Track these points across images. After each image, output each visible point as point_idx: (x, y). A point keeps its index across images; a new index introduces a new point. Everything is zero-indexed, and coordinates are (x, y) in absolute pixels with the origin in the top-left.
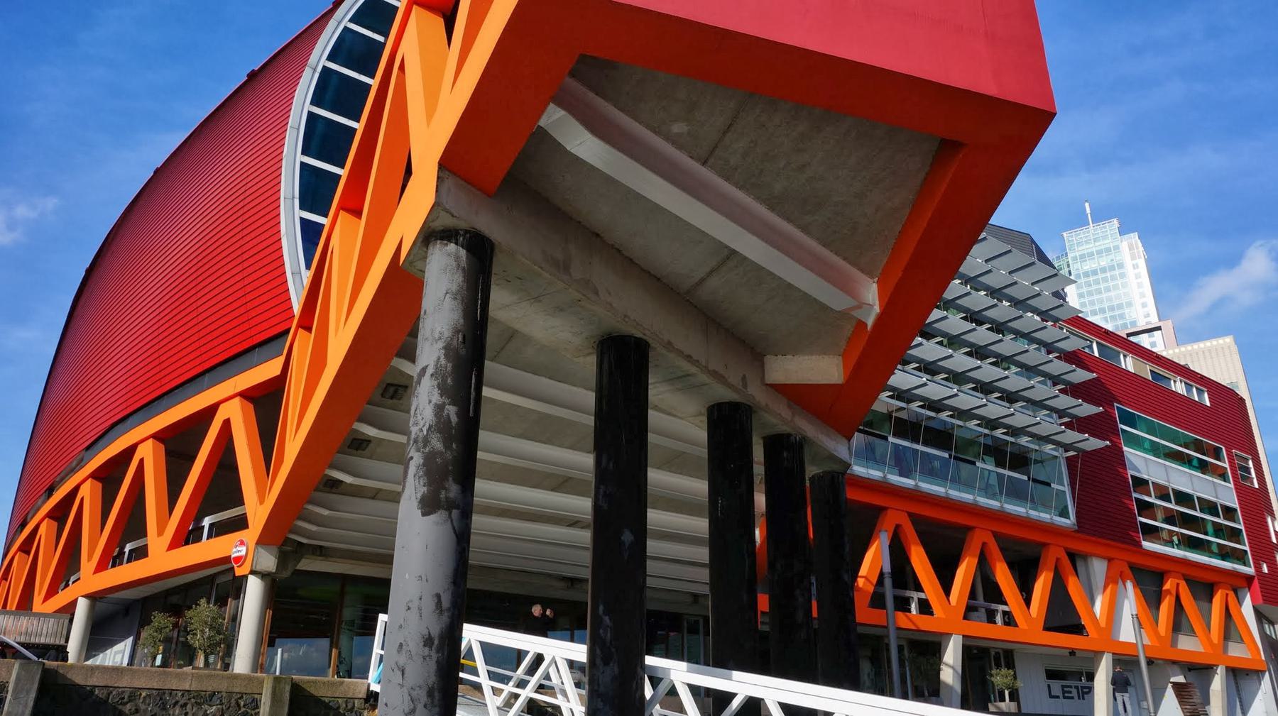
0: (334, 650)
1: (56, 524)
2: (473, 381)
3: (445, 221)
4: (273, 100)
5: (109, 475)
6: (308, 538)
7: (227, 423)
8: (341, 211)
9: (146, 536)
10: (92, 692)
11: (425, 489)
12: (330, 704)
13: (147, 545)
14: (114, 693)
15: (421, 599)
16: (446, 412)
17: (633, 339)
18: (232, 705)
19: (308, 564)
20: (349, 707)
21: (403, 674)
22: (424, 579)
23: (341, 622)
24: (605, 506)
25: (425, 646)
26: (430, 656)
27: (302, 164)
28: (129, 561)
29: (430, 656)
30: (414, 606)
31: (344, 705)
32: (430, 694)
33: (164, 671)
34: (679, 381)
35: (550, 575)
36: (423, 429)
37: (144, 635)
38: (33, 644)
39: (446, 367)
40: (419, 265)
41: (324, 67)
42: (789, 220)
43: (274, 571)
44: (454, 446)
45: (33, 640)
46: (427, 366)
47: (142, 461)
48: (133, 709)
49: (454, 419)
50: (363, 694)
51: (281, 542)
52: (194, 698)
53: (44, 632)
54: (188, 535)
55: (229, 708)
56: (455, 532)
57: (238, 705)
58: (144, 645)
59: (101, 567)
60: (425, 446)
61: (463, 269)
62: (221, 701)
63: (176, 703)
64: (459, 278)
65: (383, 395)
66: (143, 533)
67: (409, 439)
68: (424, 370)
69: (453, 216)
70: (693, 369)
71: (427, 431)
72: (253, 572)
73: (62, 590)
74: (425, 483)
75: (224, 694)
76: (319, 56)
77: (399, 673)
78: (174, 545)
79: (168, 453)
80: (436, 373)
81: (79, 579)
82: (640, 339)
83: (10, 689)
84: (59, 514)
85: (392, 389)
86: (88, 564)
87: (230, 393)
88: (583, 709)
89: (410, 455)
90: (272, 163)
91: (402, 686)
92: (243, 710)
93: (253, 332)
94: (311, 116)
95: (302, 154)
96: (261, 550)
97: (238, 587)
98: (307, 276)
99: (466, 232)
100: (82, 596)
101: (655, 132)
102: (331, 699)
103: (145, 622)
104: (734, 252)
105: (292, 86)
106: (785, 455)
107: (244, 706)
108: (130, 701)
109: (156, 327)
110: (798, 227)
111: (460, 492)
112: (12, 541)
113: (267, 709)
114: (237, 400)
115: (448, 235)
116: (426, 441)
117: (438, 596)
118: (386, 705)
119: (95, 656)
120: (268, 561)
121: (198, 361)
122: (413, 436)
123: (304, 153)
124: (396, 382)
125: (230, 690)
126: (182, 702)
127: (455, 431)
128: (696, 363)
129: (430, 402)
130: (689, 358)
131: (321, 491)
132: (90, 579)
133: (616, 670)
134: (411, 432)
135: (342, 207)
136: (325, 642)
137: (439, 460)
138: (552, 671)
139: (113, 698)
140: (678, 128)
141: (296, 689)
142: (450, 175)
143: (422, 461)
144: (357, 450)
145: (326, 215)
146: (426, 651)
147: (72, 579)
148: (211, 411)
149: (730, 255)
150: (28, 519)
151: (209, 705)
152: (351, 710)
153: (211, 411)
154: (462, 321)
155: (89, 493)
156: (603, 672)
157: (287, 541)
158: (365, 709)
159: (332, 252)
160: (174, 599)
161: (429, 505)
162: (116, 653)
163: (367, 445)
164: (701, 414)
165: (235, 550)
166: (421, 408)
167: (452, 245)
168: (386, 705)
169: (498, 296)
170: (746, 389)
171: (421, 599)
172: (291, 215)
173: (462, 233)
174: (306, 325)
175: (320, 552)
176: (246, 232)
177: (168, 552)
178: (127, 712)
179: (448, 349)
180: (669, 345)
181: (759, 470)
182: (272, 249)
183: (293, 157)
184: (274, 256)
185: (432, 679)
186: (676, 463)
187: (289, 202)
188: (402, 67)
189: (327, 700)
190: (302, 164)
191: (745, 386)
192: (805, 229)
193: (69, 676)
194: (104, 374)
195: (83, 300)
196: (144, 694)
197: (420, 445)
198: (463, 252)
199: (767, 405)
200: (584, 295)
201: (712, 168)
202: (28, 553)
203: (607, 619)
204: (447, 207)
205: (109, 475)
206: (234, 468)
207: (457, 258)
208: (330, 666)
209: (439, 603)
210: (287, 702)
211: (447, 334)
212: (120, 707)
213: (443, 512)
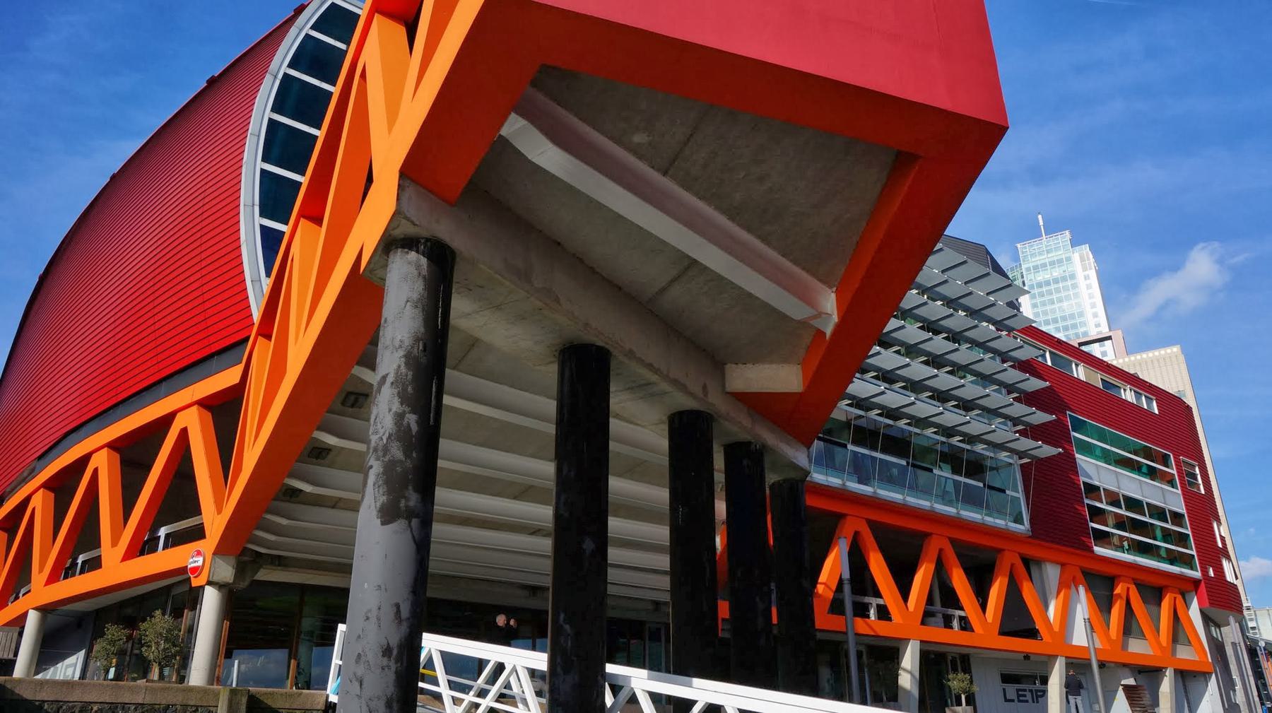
0: (292, 661)
2: (434, 389)
3: (405, 229)
4: (179, 196)
5: (62, 485)
7: (184, 432)
10: (41, 707)
11: (385, 498)
13: (100, 556)
14: (64, 707)
16: (406, 420)
19: (266, 574)
21: (361, 685)
25: (383, 656)
26: (389, 667)
28: (82, 572)
29: (389, 667)
34: (640, 389)
37: (96, 648)
39: (407, 376)
41: (285, 75)
44: (414, 455)
47: (96, 470)
49: (414, 428)
54: (143, 546)
59: (52, 579)
60: (384, 456)
61: (424, 277)
65: (343, 403)
66: (97, 545)
68: (384, 378)
69: (415, 225)
70: (654, 378)
72: (210, 583)
73: (12, 602)
75: (179, 707)
76: (281, 63)
77: (357, 684)
78: (128, 556)
79: (124, 462)
81: (29, 591)
85: (352, 398)
86: (38, 577)
87: (189, 402)
89: (370, 464)
91: (359, 697)
96: (219, 561)
97: (194, 598)
98: (267, 284)
99: (427, 240)
100: (33, 609)
103: (99, 633)
104: (694, 262)
114: (195, 408)
115: (409, 243)
116: (386, 450)
117: (398, 606)
120: (226, 572)
123: (265, 159)
124: (357, 391)
125: (185, 702)
128: (657, 371)
130: (650, 366)
134: (370, 441)
140: (639, 138)
143: (382, 470)
146: (385, 661)
147: (23, 591)
149: (691, 265)
153: (167, 420)
154: (422, 330)
155: (40, 504)
159: (292, 260)
160: (129, 611)
161: (388, 514)
162: (68, 666)
164: (663, 422)
165: (191, 560)
169: (459, 304)
171: (379, 609)
173: (423, 241)
175: (279, 562)
179: (408, 356)
180: (630, 354)
181: (719, 477)
184: (236, 272)
185: (391, 690)
186: (635, 470)
187: (249, 209)
192: (765, 239)
195: (35, 307)
197: (380, 453)
198: (424, 261)
203: (567, 627)
205: (62, 485)
207: (418, 267)
208: (288, 678)
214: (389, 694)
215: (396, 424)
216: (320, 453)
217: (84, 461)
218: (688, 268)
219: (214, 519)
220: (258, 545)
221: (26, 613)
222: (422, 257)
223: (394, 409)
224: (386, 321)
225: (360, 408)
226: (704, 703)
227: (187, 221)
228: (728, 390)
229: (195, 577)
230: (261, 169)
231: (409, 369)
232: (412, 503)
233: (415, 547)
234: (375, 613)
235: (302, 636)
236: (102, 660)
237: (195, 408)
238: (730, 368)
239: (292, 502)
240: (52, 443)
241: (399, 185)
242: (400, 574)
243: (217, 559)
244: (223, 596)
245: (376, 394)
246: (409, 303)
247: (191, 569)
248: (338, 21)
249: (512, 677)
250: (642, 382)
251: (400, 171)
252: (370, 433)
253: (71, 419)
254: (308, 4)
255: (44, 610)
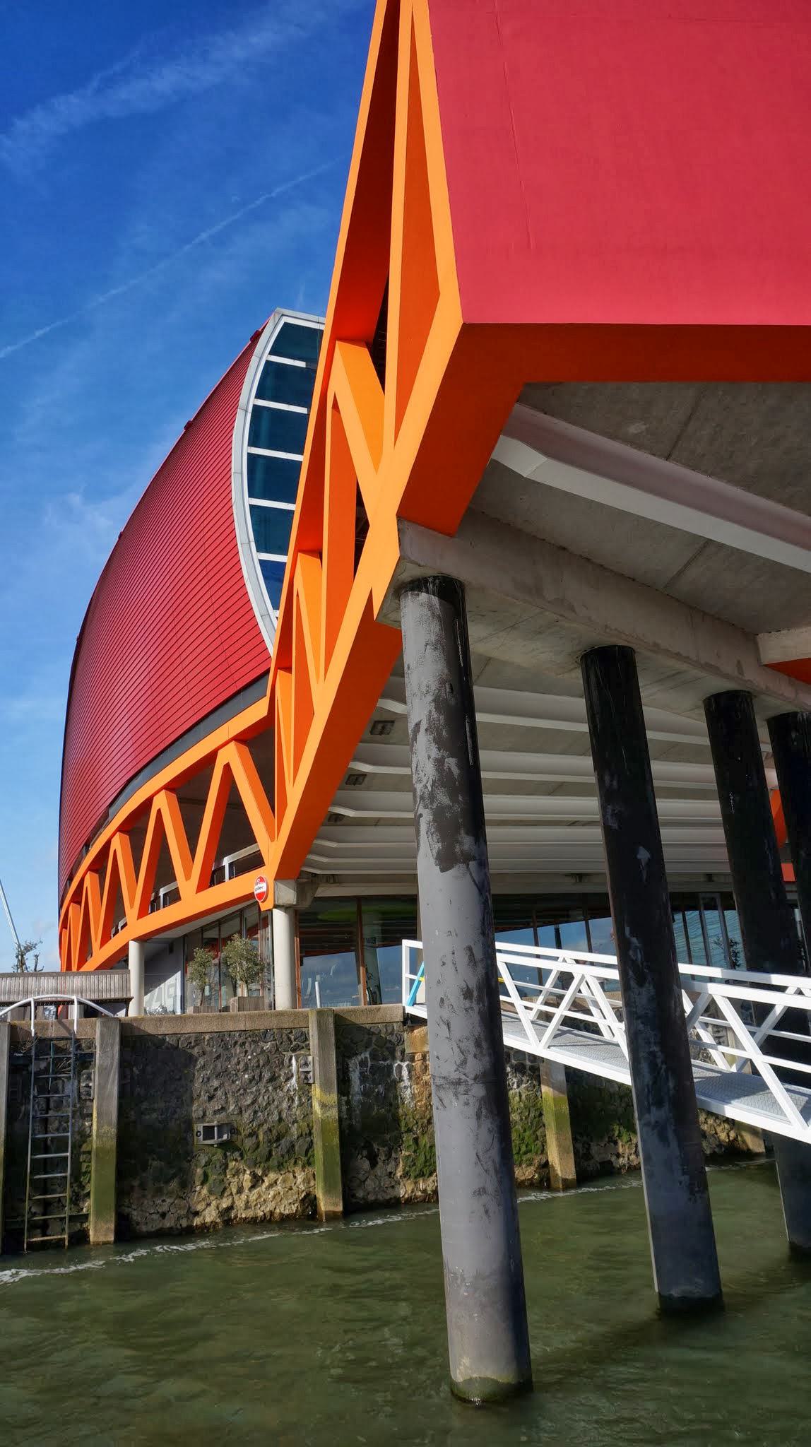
0: (361, 968)
1: (97, 876)
2: (468, 729)
3: (412, 572)
5: (134, 826)
6: (321, 869)
7: (227, 768)
8: (299, 554)
9: (176, 880)
10: (164, 1040)
11: (440, 845)
12: (372, 1030)
14: (182, 1039)
15: (453, 953)
16: (446, 765)
17: (617, 648)
18: (284, 1040)
19: (324, 891)
20: (389, 1031)
21: (449, 1028)
22: (453, 934)
23: (362, 942)
24: (615, 826)
25: (465, 998)
26: (472, 1008)
27: (252, 507)
29: (472, 1008)
30: (448, 961)
31: (385, 1030)
32: (478, 1044)
33: (221, 1015)
34: (671, 679)
35: (556, 874)
36: (427, 785)
37: (190, 970)
38: (106, 1000)
39: (439, 720)
40: (393, 616)
41: (255, 406)
42: (768, 496)
43: (295, 903)
44: (460, 798)
45: (104, 997)
46: (420, 721)
47: (159, 811)
48: (201, 1051)
49: (456, 771)
50: (400, 1018)
51: (296, 877)
52: (250, 1036)
53: (113, 988)
54: (212, 877)
55: (282, 1043)
56: (475, 884)
57: (289, 1039)
58: (192, 979)
59: (142, 914)
60: (432, 803)
61: (439, 617)
62: (274, 1037)
63: (236, 1043)
64: (435, 627)
65: (372, 732)
66: (173, 878)
67: (415, 796)
68: (418, 725)
69: (419, 566)
70: (684, 667)
71: (432, 787)
72: (276, 906)
73: (114, 935)
74: (438, 839)
75: (275, 1031)
76: (248, 396)
77: (445, 1027)
78: (201, 887)
79: (181, 801)
80: (430, 727)
82: (623, 647)
83: (98, 1044)
84: (98, 866)
85: (379, 727)
86: (131, 911)
87: (226, 739)
88: (623, 1026)
89: (419, 813)
90: (223, 511)
91: (449, 1039)
92: (294, 1043)
93: (236, 677)
94: (252, 458)
95: (249, 497)
96: (281, 886)
97: (266, 920)
98: (277, 615)
99: (435, 578)
100: (132, 940)
101: (610, 438)
102: (371, 1025)
103: (189, 958)
104: (709, 542)
105: (228, 432)
106: (793, 736)
107: (295, 1040)
108: (197, 1045)
109: (149, 685)
110: (780, 501)
111: (473, 843)
112: (63, 896)
113: (316, 1041)
114: (233, 743)
115: (417, 585)
116: (432, 797)
117: (470, 949)
118: (438, 1057)
119: (152, 991)
120: (288, 895)
121: (191, 712)
122: (419, 793)
123: (251, 495)
124: (383, 719)
125: (280, 1026)
126: (240, 1041)
127: (459, 783)
128: (686, 659)
129: (429, 757)
130: (678, 656)
131: (326, 825)
132: (136, 925)
133: (652, 991)
134: (415, 789)
135: (299, 550)
136: (351, 956)
137: (448, 815)
138: (583, 988)
139: (182, 1044)
140: (634, 429)
141: (339, 1020)
142: (409, 524)
143: (432, 817)
144: (354, 785)
145: (286, 553)
146: (467, 1003)
147: (121, 924)
148: (211, 758)
149: (706, 545)
150: (74, 873)
151: (264, 1042)
152: (392, 1033)
153: (211, 758)
154: (446, 671)
155: (119, 845)
156: (639, 994)
157: (301, 874)
158: (404, 1031)
159: (298, 595)
160: (212, 934)
161: (446, 861)
162: (169, 987)
163: (363, 780)
164: (697, 707)
165: (256, 887)
166: (421, 764)
167: (424, 594)
168: (438, 1057)
169: (475, 631)
170: (743, 675)
171: (453, 953)
172: (250, 559)
173: (430, 580)
174: (284, 663)
175: (333, 879)
176: (209, 567)
177: (140, 920)
178: (196, 1054)
179: (437, 701)
180: (656, 648)
181: (766, 748)
182: (240, 603)
183: (242, 502)
184: (247, 617)
185: (478, 1030)
186: (676, 752)
187: (246, 547)
188: (335, 406)
189: (367, 1026)
190: (252, 507)
191: (741, 673)
192: (788, 503)
193: (142, 1027)
194: (111, 736)
195: (80, 666)
196: (207, 1037)
197: (428, 801)
198: (435, 600)
199: (767, 687)
200: (561, 616)
201: (677, 461)
202: (79, 903)
203: (634, 940)
204: (413, 559)
205: (134, 826)
206: (240, 806)
207: (431, 607)
208: (359, 983)
209: (472, 956)
210: (333, 1033)
211: (434, 686)
212: (189, 1051)
213: (461, 865)
214: (476, 1034)
215: (437, 770)
216: (357, 780)
217: (148, 803)
218: (705, 547)
219: (271, 847)
220: (314, 867)
221: (128, 943)
222: (433, 597)
223: (433, 756)
224: (409, 668)
225: (388, 734)
226: (786, 992)
227: (184, 542)
228: (766, 661)
229: (263, 902)
230: (250, 505)
231: (440, 713)
232: (466, 847)
233: (477, 891)
234: (450, 957)
235: (366, 944)
236: (197, 981)
237: (233, 743)
238: (762, 638)
239: (337, 825)
240: (118, 791)
241: (399, 530)
242: (467, 918)
243: (280, 885)
244: (290, 920)
245: (413, 742)
246: (428, 646)
247: (258, 894)
248: (293, 340)
249: (582, 985)
250: (674, 672)
251: (397, 515)
252: (414, 782)
253: (129, 767)
254: (263, 330)
255: (142, 940)
